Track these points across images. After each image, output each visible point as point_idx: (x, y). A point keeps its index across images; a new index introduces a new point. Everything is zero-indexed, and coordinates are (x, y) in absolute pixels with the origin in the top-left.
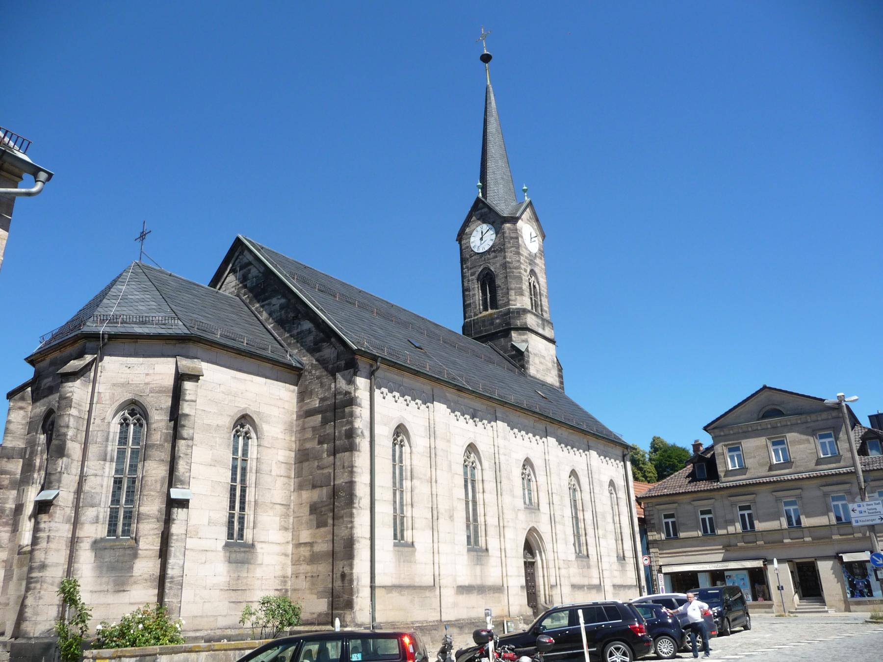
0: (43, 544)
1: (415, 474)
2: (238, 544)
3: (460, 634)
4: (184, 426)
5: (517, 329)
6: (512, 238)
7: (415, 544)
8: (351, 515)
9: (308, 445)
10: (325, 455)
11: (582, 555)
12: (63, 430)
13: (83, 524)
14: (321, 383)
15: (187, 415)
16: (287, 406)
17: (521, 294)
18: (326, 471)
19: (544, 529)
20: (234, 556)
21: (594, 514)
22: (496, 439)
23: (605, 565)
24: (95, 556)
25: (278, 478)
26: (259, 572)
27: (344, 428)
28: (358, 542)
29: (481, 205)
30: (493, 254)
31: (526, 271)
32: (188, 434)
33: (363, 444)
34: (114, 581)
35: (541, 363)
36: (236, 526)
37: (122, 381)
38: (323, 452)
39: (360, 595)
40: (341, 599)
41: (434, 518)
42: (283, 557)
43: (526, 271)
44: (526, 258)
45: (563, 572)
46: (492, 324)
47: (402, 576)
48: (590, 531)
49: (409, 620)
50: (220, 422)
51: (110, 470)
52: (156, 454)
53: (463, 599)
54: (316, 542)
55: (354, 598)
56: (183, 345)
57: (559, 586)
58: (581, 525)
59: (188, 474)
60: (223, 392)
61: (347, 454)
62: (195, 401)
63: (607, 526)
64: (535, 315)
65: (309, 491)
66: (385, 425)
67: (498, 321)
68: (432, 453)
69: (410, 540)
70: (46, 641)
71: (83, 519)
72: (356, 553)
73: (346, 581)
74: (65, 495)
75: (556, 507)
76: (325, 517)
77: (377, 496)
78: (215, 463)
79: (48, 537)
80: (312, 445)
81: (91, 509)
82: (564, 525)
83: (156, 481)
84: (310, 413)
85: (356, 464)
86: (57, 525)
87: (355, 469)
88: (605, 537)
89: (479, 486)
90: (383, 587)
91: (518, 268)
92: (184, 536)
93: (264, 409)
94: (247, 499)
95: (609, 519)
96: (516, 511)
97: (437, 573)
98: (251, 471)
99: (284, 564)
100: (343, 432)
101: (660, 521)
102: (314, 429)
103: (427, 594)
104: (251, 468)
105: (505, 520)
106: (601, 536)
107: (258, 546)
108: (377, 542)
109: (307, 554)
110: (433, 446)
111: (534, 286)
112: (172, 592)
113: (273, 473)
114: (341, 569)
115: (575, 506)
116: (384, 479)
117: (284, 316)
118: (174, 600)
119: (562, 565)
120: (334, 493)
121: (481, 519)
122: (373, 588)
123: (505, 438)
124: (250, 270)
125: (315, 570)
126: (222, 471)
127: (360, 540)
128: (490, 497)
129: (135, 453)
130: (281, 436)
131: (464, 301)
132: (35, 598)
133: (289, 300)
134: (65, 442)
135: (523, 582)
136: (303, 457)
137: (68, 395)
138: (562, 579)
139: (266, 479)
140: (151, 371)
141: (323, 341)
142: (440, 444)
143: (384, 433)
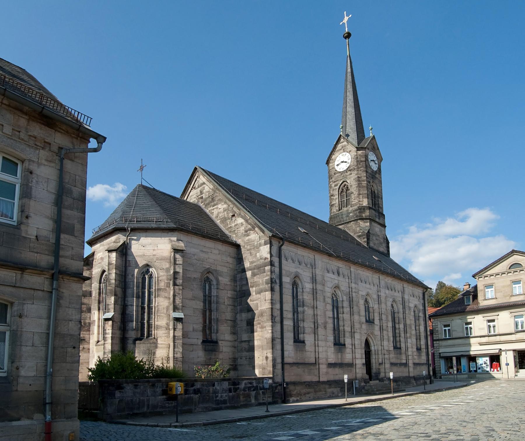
1: (305, 304)
7: (306, 342)
13: (128, 331)
14: (251, 253)
16: (231, 266)
18: (255, 302)
23: (410, 353)
29: (342, 140)
30: (349, 173)
35: (376, 239)
37: (141, 254)
38: (253, 292)
46: (348, 216)
47: (299, 358)
48: (402, 335)
50: (195, 276)
53: (331, 370)
58: (397, 331)
60: (196, 259)
64: (374, 210)
66: (288, 276)
67: (351, 214)
68: (314, 292)
75: (384, 321)
88: (410, 337)
89: (341, 310)
93: (219, 268)
95: (413, 328)
96: (361, 323)
97: (317, 357)
101: (441, 329)
103: (312, 367)
104: (214, 301)
107: (220, 342)
109: (247, 347)
110: (315, 288)
113: (226, 304)
114: (266, 355)
117: (226, 216)
119: (386, 353)
121: (341, 328)
123: (355, 283)
124: (204, 188)
126: (198, 302)
130: (229, 283)
133: (229, 205)
135: (364, 361)
138: (386, 360)
140: (156, 248)
141: (250, 230)
142: (319, 287)
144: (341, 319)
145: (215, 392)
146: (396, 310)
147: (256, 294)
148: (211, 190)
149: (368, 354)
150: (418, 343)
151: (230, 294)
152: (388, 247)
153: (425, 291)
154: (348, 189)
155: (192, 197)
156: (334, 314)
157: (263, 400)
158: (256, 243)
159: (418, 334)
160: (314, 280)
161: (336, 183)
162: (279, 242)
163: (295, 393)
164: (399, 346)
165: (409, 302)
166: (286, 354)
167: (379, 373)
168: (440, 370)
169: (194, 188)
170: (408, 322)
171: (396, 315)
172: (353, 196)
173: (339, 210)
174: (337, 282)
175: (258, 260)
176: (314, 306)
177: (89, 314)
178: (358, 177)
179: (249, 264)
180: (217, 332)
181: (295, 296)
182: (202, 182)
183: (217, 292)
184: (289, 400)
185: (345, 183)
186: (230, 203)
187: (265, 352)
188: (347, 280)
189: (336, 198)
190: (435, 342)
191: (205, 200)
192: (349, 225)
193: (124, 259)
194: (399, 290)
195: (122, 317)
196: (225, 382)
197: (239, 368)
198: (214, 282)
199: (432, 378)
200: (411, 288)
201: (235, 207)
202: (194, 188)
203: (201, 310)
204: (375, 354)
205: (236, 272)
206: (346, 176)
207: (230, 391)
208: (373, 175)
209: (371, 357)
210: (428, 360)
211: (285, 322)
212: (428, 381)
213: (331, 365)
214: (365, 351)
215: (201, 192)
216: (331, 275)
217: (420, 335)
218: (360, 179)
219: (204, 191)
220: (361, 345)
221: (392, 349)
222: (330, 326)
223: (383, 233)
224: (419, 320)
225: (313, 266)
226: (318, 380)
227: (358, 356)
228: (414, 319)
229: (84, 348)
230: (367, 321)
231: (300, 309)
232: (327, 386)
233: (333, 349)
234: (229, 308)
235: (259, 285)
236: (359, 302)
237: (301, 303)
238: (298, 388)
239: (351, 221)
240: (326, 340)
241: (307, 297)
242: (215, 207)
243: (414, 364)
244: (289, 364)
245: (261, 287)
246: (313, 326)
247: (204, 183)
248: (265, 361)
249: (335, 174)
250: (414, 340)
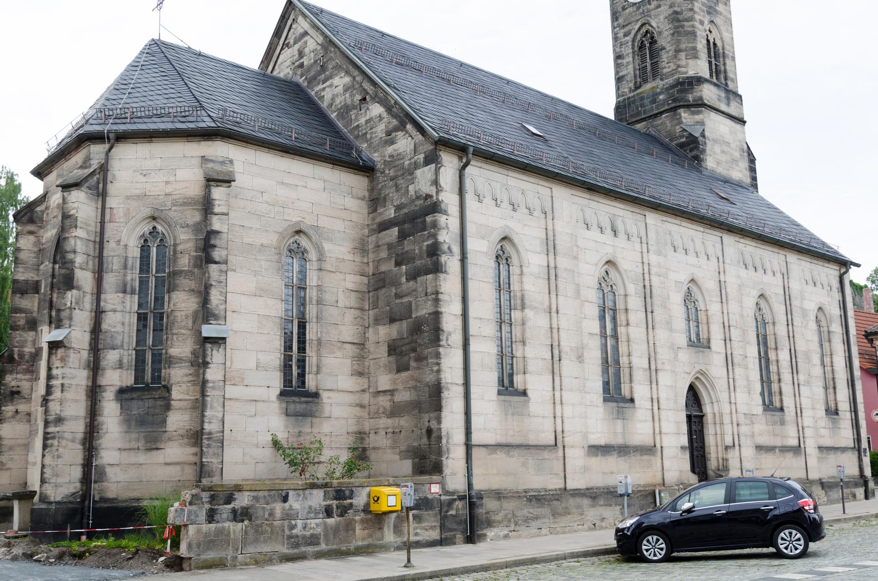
0: (57, 394)
1: (527, 302)
2: (298, 392)
3: (593, 506)
4: (215, 246)
5: (688, 106)
7: (529, 392)
8: (438, 355)
9: (384, 268)
10: (404, 280)
11: (772, 406)
12: (70, 256)
13: (104, 369)
14: (397, 186)
15: (218, 232)
16: (355, 217)
18: (405, 300)
19: (717, 369)
20: (292, 407)
21: (793, 354)
22: (645, 255)
24: (121, 408)
25: (347, 311)
26: (326, 427)
27: (425, 244)
28: (448, 389)
31: (702, 23)
32: (220, 256)
33: (452, 264)
34: (145, 437)
35: (723, 152)
36: (295, 371)
37: (138, 192)
38: (401, 276)
39: (451, 455)
40: (428, 461)
41: (555, 358)
42: (358, 409)
43: (702, 23)
45: (744, 429)
46: (654, 101)
47: (511, 432)
48: (786, 376)
49: (521, 487)
50: (265, 241)
51: (132, 303)
52: (185, 283)
53: (598, 462)
54: (397, 390)
55: (444, 459)
56: (210, 143)
57: (737, 447)
58: (773, 368)
59: (223, 307)
60: (267, 202)
61: (430, 276)
62: (227, 214)
63: (812, 369)
64: (715, 85)
65: (387, 326)
66: (483, 238)
67: (661, 97)
68: (551, 275)
69: (778, 405)
70: (71, 506)
71: (103, 363)
72: (444, 403)
73: (433, 439)
74: (78, 334)
75: (735, 344)
76: (406, 358)
77: (472, 330)
78: (260, 293)
79: (62, 385)
80: (388, 266)
81: (112, 352)
83: (187, 317)
84: (384, 226)
86: (72, 371)
87: (441, 296)
88: (808, 383)
89: (621, 318)
90: (483, 446)
91: (691, 19)
92: (222, 384)
93: (324, 222)
94: (307, 338)
95: (816, 360)
97: (559, 429)
98: (311, 301)
99: (360, 417)
100: (424, 248)
102: (390, 246)
103: (546, 454)
105: (659, 362)
106: (802, 382)
107: (324, 395)
108: (473, 390)
109: (388, 405)
110: (552, 265)
111: (715, 44)
112: (211, 451)
113: (340, 304)
114: (427, 424)
115: (766, 344)
116: (483, 307)
117: (349, 101)
118: (214, 460)
119: (742, 419)
120: (417, 328)
121: (624, 360)
122: (469, 446)
123: (659, 253)
124: (306, 43)
125: (396, 425)
126: (271, 302)
129: (160, 282)
130: (349, 257)
131: (617, 73)
132: (53, 457)
133: (354, 78)
134: (73, 270)
135: (684, 440)
136: (378, 282)
137: (72, 212)
138: (742, 439)
139: (331, 313)
140: (172, 179)
141: (396, 129)
142: (563, 262)
143: (481, 249)
145: (289, 516)
146: (769, 318)
147: (408, 280)
148: (319, 48)
149: (696, 422)
151: (352, 281)
153: (843, 270)
154: (653, 42)
155: (283, 67)
156: (603, 327)
157: (416, 534)
158: (407, 163)
159: (829, 376)
160: (550, 246)
161: (626, 29)
162: (460, 158)
163: (498, 518)
164: (778, 405)
165: (803, 299)
166: (476, 422)
167: (726, 469)
169: (286, 45)
170: (801, 346)
171: (770, 329)
173: (637, 88)
174: (610, 250)
175: (413, 201)
176: (550, 309)
177: (32, 333)
178: (676, 13)
179: (393, 211)
180: (318, 372)
181: (503, 286)
182: (302, 31)
183: (319, 279)
184: (485, 535)
185: (647, 27)
186: (356, 73)
187: (426, 417)
188: (638, 246)
189: (628, 63)
191: (309, 70)
192: (658, 122)
193: (100, 206)
194: (776, 268)
195: (91, 339)
196: (315, 492)
197: (373, 455)
198: (313, 255)
201: (365, 81)
202: (287, 45)
203: (278, 320)
205: (366, 231)
206: (649, 11)
207: (328, 512)
208: (710, 7)
209: (705, 431)
211: (475, 346)
212: (860, 492)
214: (689, 417)
215: (301, 54)
217: (834, 379)
218: (680, 17)
219: (307, 50)
220: (676, 401)
221: (759, 409)
222: (594, 355)
223: (740, 136)
225: (548, 213)
226: (562, 486)
228: (816, 339)
229: (17, 412)
230: (691, 344)
231: (516, 315)
232: (586, 502)
234: (347, 315)
237: (519, 302)
238: (509, 506)
239: (661, 113)
242: (327, 84)
245: (418, 263)
246: (548, 356)
247: (306, 33)
248: (425, 440)
249: (624, 9)
250: (820, 391)
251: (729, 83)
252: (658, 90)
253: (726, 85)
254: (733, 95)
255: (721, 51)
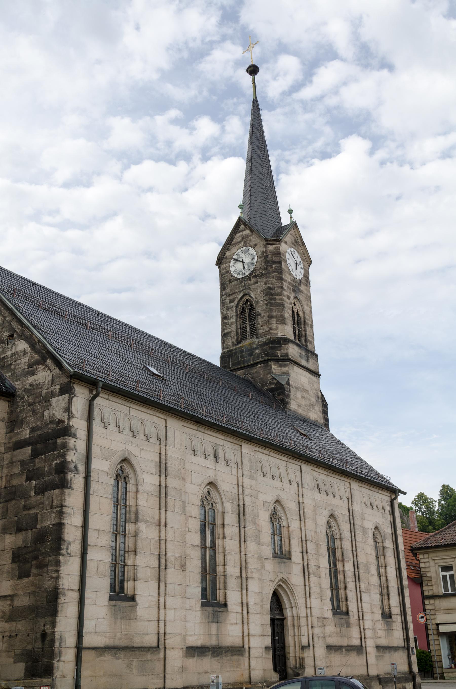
1: (140, 516)
5: (277, 360)
6: (274, 262)
7: (138, 598)
8: (58, 563)
9: (15, 482)
10: (33, 493)
11: (340, 611)
14: (34, 411)
17: (283, 321)
18: (33, 511)
19: (296, 579)
21: (356, 565)
22: (240, 478)
23: (368, 624)
28: (64, 595)
29: (242, 227)
30: (253, 280)
31: (289, 298)
33: (77, 481)
35: (303, 397)
38: (31, 489)
39: (63, 658)
43: (289, 298)
44: (290, 284)
46: (251, 354)
47: (119, 635)
48: (351, 585)
53: (193, 663)
55: (55, 662)
57: (311, 647)
58: (340, 577)
61: (56, 491)
64: (298, 345)
66: (106, 459)
67: (257, 351)
68: (162, 493)
72: (59, 609)
73: (47, 642)
75: (311, 556)
76: (29, 565)
82: (319, 577)
85: (66, 504)
87: (65, 509)
88: (368, 591)
89: (219, 531)
91: (281, 294)
95: (374, 571)
96: (262, 559)
97: (162, 632)
100: (54, 466)
101: (437, 574)
102: (23, 463)
103: (149, 656)
105: (249, 571)
106: (363, 590)
108: (88, 595)
109: (7, 609)
110: (163, 484)
111: (298, 314)
114: (42, 628)
119: (316, 622)
120: (40, 538)
121: (220, 569)
122: (79, 649)
123: (251, 477)
125: (13, 629)
127: (66, 592)
128: (231, 544)
131: (223, 330)
133: (5, 318)
135: (268, 641)
138: (316, 639)
142: (173, 482)
143: (103, 468)
144: (219, 549)
146: (337, 535)
147: (36, 494)
149: (278, 625)
150: (386, 603)
152: (325, 413)
153: (393, 497)
154: (252, 308)
156: (204, 539)
158: (45, 391)
160: (162, 468)
161: (231, 297)
162: (91, 391)
165: (363, 519)
166: (88, 625)
167: (302, 667)
168: (441, 661)
170: (362, 559)
172: (260, 321)
173: (238, 343)
174: (211, 473)
175: (46, 425)
176: (160, 522)
178: (269, 288)
179: (28, 432)
181: (120, 501)
185: (248, 297)
186: (7, 314)
188: (234, 471)
189: (232, 323)
190: (426, 602)
192: (254, 370)
194: (343, 493)
199: (418, 679)
200: (367, 491)
204: (294, 626)
206: (249, 285)
208: (295, 287)
209: (286, 633)
210: (407, 640)
211: (91, 555)
213: (194, 651)
214: (272, 620)
216: (199, 459)
217: (387, 587)
218: (273, 292)
220: (262, 606)
221: (329, 614)
222: (195, 564)
223: (316, 386)
224: (384, 555)
225: (163, 440)
227: (255, 629)
228: (373, 553)
230: (275, 556)
233: (199, 614)
235: (42, 475)
236: (258, 516)
237: (133, 516)
239: (257, 364)
240: (184, 596)
241: (146, 503)
243: (378, 648)
244: (94, 648)
245: (47, 478)
246: (156, 565)
248: (39, 644)
249: (230, 281)
250: (377, 598)
251: (308, 344)
252: (255, 346)
253: (306, 346)
254: (311, 354)
255: (302, 320)
